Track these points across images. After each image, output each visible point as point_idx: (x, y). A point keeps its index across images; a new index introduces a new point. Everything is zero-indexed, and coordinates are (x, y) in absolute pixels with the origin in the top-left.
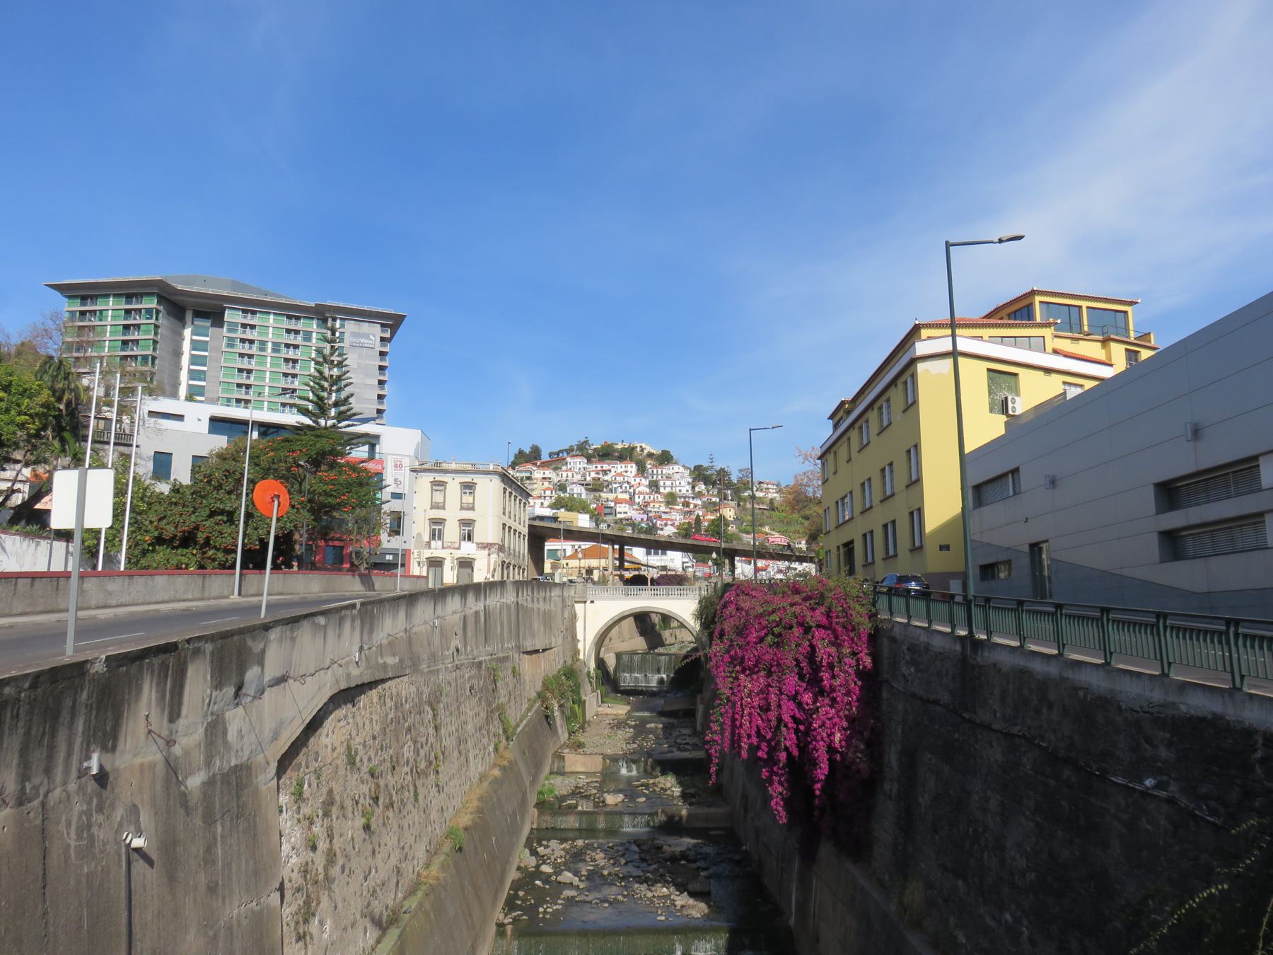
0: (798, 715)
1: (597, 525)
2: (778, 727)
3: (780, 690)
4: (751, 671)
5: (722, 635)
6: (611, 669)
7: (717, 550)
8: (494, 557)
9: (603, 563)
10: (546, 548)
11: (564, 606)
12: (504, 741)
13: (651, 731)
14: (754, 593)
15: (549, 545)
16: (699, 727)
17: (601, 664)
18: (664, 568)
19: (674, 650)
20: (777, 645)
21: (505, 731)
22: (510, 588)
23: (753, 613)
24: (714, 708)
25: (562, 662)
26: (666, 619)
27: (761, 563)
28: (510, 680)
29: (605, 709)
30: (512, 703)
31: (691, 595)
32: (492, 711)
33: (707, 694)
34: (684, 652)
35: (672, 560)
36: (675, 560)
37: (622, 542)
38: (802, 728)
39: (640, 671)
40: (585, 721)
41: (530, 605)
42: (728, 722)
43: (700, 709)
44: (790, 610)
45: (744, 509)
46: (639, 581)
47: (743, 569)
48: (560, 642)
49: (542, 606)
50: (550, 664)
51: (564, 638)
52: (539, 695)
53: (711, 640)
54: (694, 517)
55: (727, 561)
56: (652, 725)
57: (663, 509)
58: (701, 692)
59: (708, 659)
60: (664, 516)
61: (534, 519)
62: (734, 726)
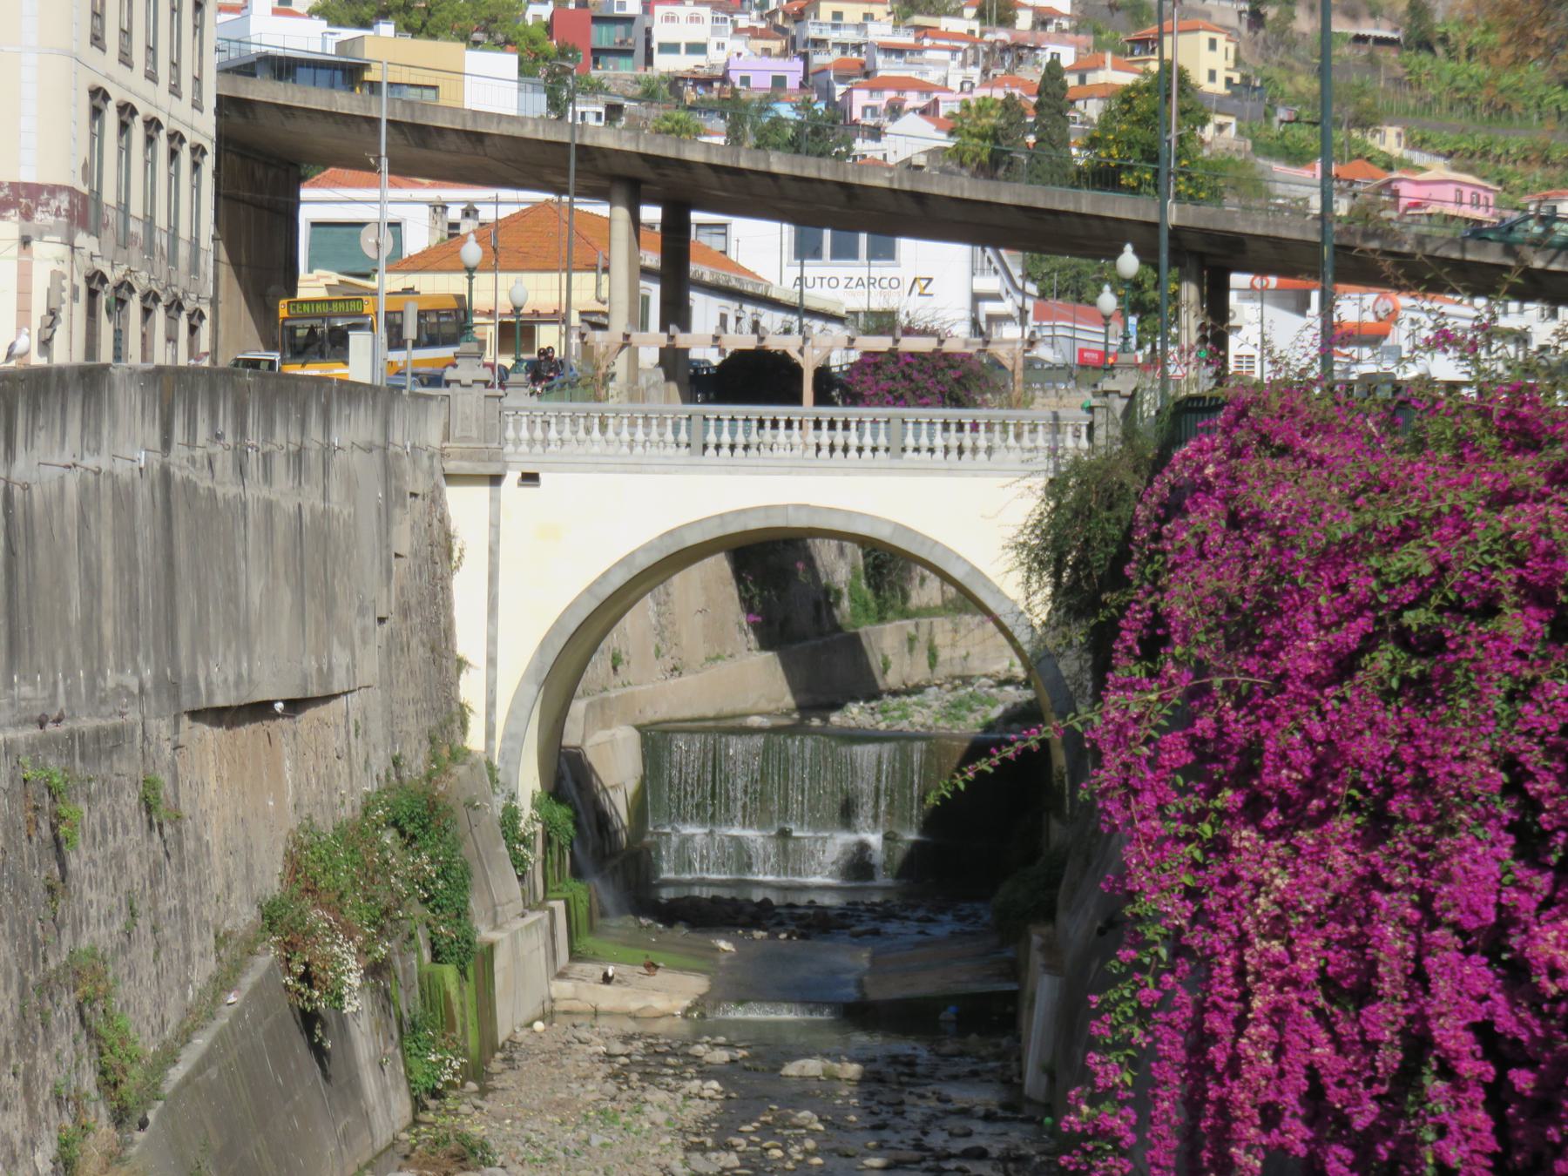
0: (1505, 1022)
1: (555, 104)
2: (1407, 1077)
3: (1425, 901)
4: (1286, 813)
5: (1153, 645)
6: (619, 805)
7: (1145, 237)
8: (49, 254)
9: (585, 290)
10: (307, 214)
11: (394, 496)
12: (104, 1128)
13: (803, 1094)
14: (1317, 445)
15: (320, 202)
16: (1033, 1081)
17: (568, 776)
18: (883, 322)
19: (922, 715)
20: (1420, 691)
21: (109, 1082)
22: (128, 402)
23: (1307, 539)
24: (1113, 981)
25: (380, 763)
26: (887, 565)
27: (1355, 306)
28: (133, 839)
29: (581, 990)
30: (143, 951)
31: (1010, 453)
32: (46, 987)
33: (1076, 925)
34: (971, 724)
35: (922, 285)
36: (938, 286)
37: (677, 193)
38: (1523, 1080)
39: (756, 813)
40: (489, 1044)
41: (228, 489)
42: (1175, 1049)
43: (1044, 991)
44: (1489, 526)
45: (1285, 39)
46: (757, 379)
47: (1269, 332)
48: (370, 666)
49: (283, 491)
50: (325, 773)
51: (394, 648)
52: (271, 917)
53: (1102, 666)
54: (1032, 74)
55: (1190, 292)
56: (813, 1066)
57: (882, 30)
58: (1048, 913)
59: (1085, 754)
60: (886, 67)
61: (247, 69)
62: (1198, 1067)
